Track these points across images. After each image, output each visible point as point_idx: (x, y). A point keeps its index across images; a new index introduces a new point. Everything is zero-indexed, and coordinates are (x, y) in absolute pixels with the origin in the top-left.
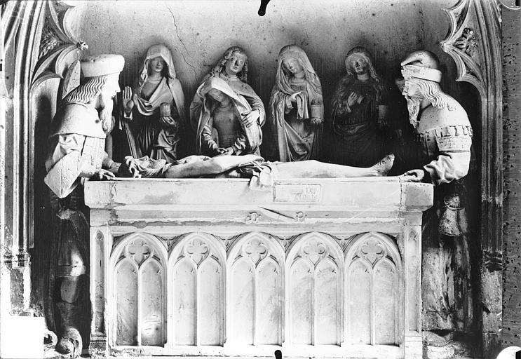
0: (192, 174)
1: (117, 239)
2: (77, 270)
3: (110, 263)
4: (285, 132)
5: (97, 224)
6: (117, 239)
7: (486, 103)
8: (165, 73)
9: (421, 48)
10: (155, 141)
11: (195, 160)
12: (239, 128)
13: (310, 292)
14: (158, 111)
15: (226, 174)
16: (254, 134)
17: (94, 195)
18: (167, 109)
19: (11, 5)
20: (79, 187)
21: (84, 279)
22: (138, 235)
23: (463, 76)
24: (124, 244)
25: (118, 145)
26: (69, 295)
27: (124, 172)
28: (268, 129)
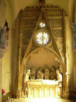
0: (37, 81)
1: (30, 87)
2: (26, 90)
3: (29, 89)
4: (46, 77)
5: (28, 86)
6: (30, 87)
7: (63, 74)
8: (34, 70)
9: (58, 69)
10: (33, 77)
11: (37, 80)
12: (41, 76)
13: (58, 7)
14: (33, 74)
15: (40, 81)
16: (43, 77)
17: (28, 83)
18: (34, 74)
19: (2, 1)
20: (27, 83)
21: (27, 91)
22: (32, 87)
23: (61, 72)
24: (31, 88)
25: (29, 78)
26: (26, 92)
27: (30, 81)
28: (44, 76)
